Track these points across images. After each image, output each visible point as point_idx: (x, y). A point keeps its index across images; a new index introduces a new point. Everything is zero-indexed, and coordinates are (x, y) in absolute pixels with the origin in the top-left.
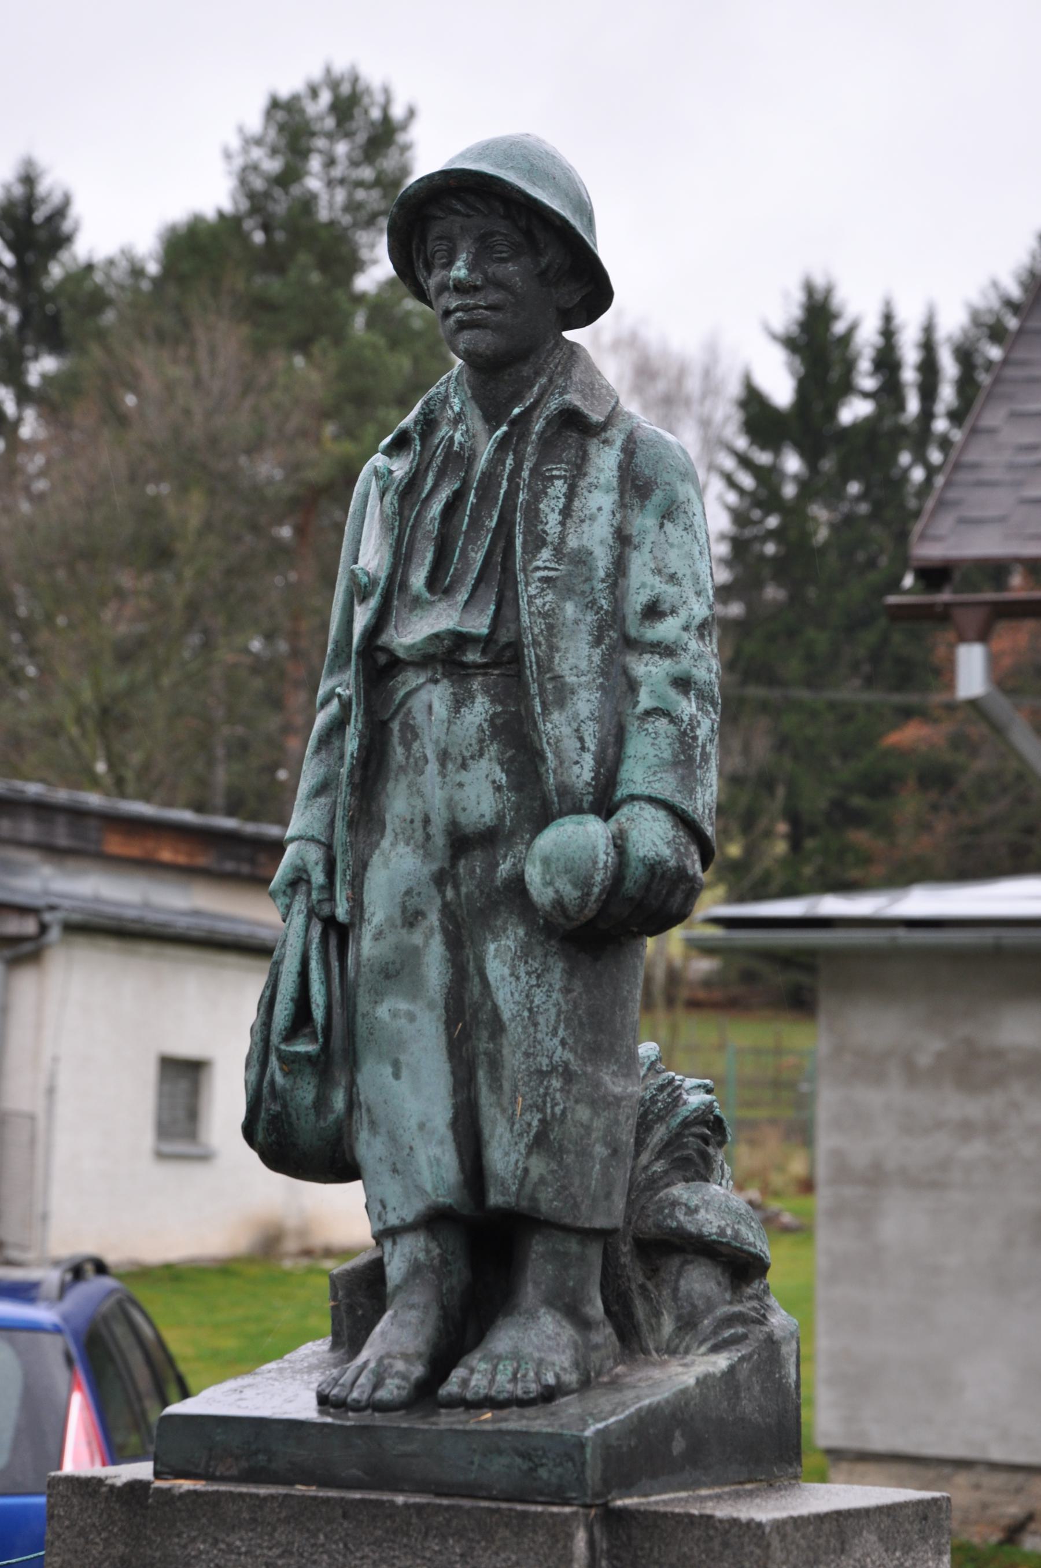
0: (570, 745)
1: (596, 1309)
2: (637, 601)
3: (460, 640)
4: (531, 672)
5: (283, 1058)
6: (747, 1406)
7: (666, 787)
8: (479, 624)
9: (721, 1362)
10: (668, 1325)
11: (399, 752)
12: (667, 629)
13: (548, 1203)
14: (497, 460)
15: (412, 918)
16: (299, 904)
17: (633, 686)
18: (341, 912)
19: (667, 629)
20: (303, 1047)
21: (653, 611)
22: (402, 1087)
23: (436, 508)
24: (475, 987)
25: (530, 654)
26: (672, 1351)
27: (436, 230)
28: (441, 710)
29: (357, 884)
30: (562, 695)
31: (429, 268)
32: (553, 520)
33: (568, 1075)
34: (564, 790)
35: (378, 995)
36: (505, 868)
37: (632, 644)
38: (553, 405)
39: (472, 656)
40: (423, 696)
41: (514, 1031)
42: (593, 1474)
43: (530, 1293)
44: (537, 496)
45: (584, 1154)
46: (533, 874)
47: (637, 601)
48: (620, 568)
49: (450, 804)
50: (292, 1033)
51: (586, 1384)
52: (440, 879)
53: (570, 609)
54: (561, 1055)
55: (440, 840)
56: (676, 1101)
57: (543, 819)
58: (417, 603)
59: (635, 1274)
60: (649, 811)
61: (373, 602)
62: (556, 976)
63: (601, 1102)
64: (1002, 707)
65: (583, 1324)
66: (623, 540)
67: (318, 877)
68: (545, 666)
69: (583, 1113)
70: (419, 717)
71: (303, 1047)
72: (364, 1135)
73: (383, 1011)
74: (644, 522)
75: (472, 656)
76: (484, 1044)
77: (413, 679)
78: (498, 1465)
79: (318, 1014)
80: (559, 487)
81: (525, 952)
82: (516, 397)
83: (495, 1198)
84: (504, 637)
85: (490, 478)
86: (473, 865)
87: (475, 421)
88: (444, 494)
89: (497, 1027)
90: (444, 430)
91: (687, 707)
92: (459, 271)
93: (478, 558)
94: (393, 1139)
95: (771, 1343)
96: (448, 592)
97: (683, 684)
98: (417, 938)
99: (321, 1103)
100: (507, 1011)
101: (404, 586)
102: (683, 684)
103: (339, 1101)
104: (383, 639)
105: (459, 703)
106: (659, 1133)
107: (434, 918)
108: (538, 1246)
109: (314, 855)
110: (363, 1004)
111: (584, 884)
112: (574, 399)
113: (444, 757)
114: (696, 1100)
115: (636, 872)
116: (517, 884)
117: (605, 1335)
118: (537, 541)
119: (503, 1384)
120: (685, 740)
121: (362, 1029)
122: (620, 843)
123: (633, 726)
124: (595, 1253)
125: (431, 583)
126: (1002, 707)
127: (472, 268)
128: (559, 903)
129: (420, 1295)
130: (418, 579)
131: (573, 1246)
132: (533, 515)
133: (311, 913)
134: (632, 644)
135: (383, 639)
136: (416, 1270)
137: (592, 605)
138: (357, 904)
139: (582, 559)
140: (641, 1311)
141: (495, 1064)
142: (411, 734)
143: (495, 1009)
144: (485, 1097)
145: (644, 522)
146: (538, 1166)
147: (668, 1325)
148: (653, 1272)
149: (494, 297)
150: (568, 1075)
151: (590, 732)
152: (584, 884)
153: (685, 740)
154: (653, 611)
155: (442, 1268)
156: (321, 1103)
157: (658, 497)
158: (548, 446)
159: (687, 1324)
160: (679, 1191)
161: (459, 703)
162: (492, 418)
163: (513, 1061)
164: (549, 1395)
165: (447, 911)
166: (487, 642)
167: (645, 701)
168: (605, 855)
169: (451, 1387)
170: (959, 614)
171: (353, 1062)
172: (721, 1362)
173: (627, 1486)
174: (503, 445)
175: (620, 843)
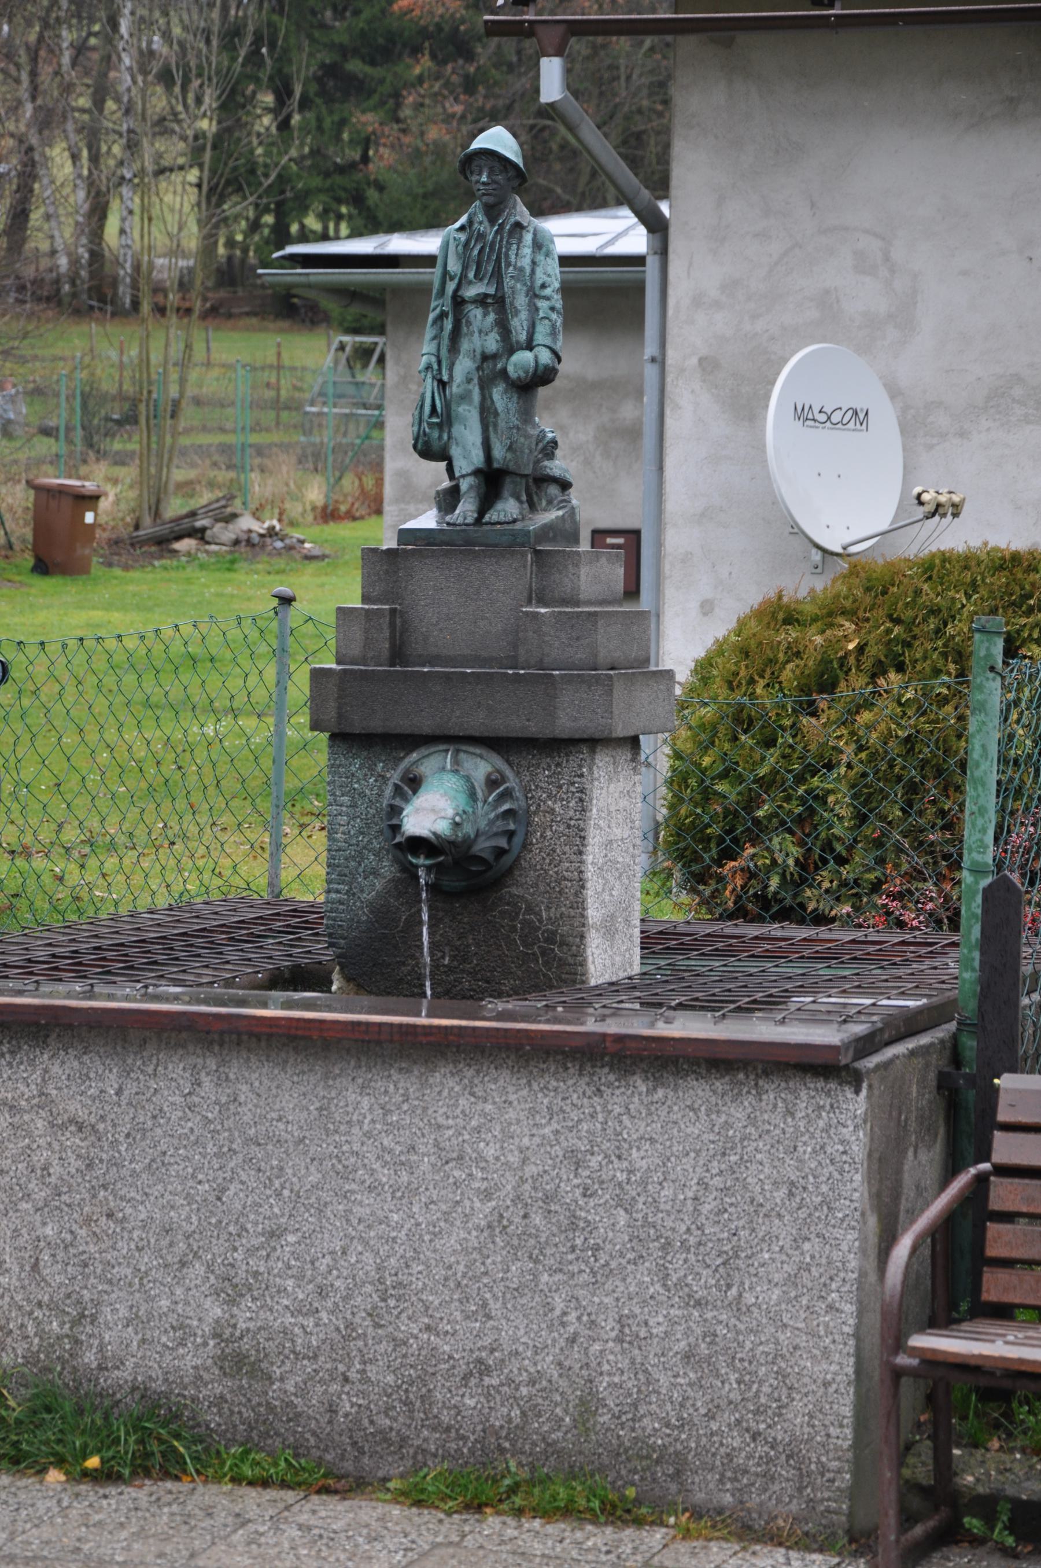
0: (519, 328)
1: (524, 498)
2: (539, 283)
3: (486, 296)
4: (508, 306)
5: (429, 424)
6: (567, 526)
7: (548, 341)
8: (492, 291)
9: (560, 513)
10: (544, 503)
11: (465, 329)
12: (548, 292)
13: (512, 466)
14: (495, 237)
15: (469, 381)
16: (429, 375)
17: (537, 309)
18: (445, 378)
19: (548, 292)
20: (435, 420)
21: (543, 286)
22: (467, 432)
23: (476, 252)
24: (489, 402)
25: (508, 301)
26: (545, 510)
27: (475, 163)
28: (479, 317)
29: (451, 370)
30: (517, 312)
31: (472, 173)
32: (513, 258)
33: (518, 429)
34: (518, 342)
35: (459, 405)
36: (499, 366)
37: (536, 296)
38: (512, 220)
39: (489, 301)
40: (473, 312)
41: (502, 415)
42: (532, 540)
43: (506, 493)
44: (508, 249)
45: (522, 452)
46: (510, 369)
47: (539, 283)
48: (533, 272)
49: (482, 346)
50: (431, 416)
51: (523, 519)
52: (478, 369)
53: (519, 286)
54: (516, 422)
55: (478, 357)
56: (545, 436)
57: (511, 351)
58: (470, 283)
59: (534, 489)
60: (544, 349)
61: (456, 281)
62: (515, 399)
63: (527, 436)
64: (575, 110)
65: (521, 502)
66: (534, 263)
67: (435, 367)
68: (512, 304)
69: (522, 440)
70: (472, 319)
71: (435, 420)
72: (454, 447)
73: (460, 409)
74: (540, 258)
75: (489, 301)
76: (492, 419)
77: (470, 307)
78: (505, 538)
79: (439, 410)
80: (515, 247)
81: (506, 392)
82: (499, 215)
83: (496, 465)
84: (499, 294)
85: (493, 243)
86: (489, 364)
87: (486, 223)
88: (478, 247)
89: (496, 414)
90: (476, 225)
91: (554, 316)
92: (484, 178)
93: (490, 269)
94: (464, 448)
95: (573, 508)
96: (481, 280)
97: (552, 309)
98: (470, 387)
99: (440, 437)
100: (500, 409)
101: (466, 276)
102: (552, 309)
103: (445, 436)
104: (460, 293)
105: (485, 315)
106: (541, 445)
107: (476, 381)
108: (508, 480)
109: (433, 359)
110: (454, 407)
111: (527, 372)
112: (518, 218)
113: (480, 332)
114: (550, 435)
115: (541, 368)
116: (504, 372)
117: (526, 506)
118: (508, 264)
119: (502, 518)
120: (553, 327)
121: (453, 414)
122: (536, 357)
123: (538, 322)
124: (524, 481)
125: (475, 276)
126: (575, 110)
127: (488, 177)
128: (519, 378)
129: (473, 494)
130: (471, 275)
131: (518, 479)
132: (507, 256)
133: (434, 378)
134: (536, 296)
135: (460, 293)
136: (471, 487)
137: (525, 284)
138: (451, 376)
139: (521, 270)
140: (535, 499)
141: (495, 425)
142: (469, 323)
143: (496, 410)
144: (492, 435)
145: (540, 258)
146: (509, 456)
147: (544, 503)
148: (538, 488)
149: (495, 186)
150: (518, 429)
151: (525, 323)
152: (527, 372)
153: (553, 327)
154: (543, 286)
155: (478, 487)
156: (440, 437)
157: (544, 250)
158: (511, 233)
159: (550, 502)
160: (546, 463)
161: (485, 315)
162: (492, 221)
163: (502, 424)
164: (515, 521)
165: (480, 378)
166: (494, 296)
167: (541, 314)
168: (533, 364)
169: (487, 518)
170: (540, 30)
171: (450, 425)
172: (560, 513)
173: (540, 543)
174: (497, 232)
175: (536, 357)
